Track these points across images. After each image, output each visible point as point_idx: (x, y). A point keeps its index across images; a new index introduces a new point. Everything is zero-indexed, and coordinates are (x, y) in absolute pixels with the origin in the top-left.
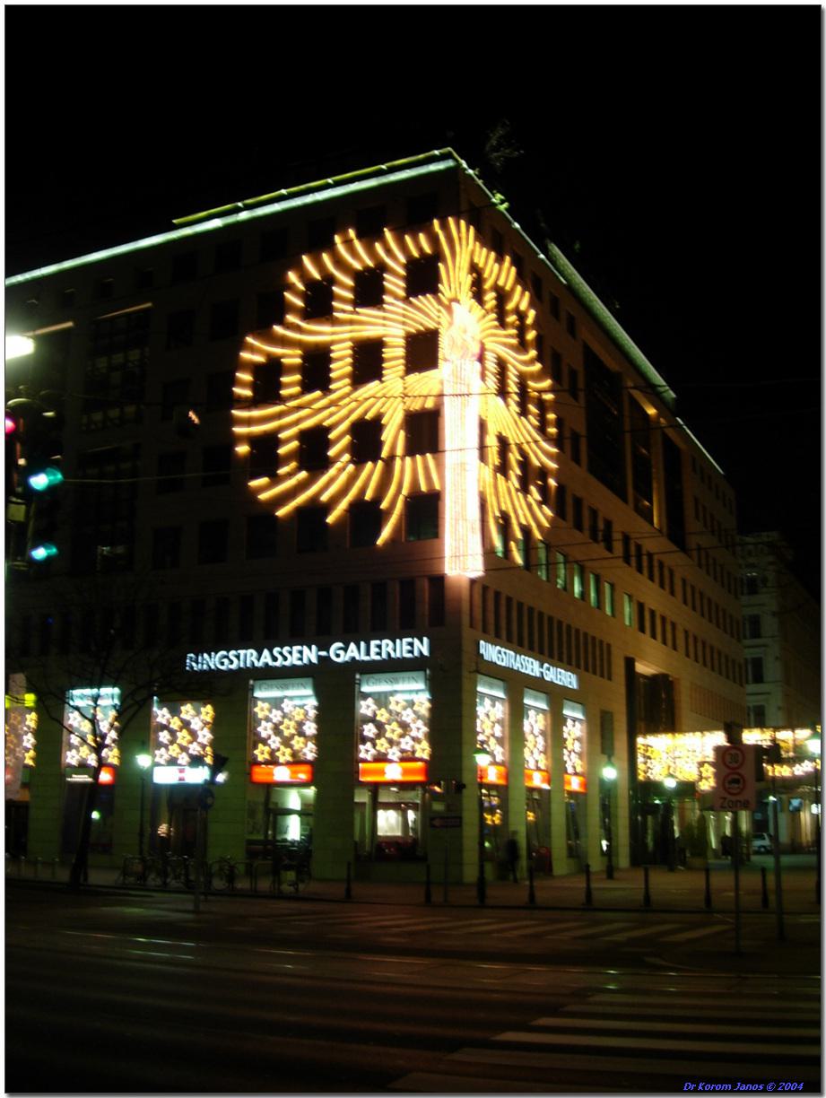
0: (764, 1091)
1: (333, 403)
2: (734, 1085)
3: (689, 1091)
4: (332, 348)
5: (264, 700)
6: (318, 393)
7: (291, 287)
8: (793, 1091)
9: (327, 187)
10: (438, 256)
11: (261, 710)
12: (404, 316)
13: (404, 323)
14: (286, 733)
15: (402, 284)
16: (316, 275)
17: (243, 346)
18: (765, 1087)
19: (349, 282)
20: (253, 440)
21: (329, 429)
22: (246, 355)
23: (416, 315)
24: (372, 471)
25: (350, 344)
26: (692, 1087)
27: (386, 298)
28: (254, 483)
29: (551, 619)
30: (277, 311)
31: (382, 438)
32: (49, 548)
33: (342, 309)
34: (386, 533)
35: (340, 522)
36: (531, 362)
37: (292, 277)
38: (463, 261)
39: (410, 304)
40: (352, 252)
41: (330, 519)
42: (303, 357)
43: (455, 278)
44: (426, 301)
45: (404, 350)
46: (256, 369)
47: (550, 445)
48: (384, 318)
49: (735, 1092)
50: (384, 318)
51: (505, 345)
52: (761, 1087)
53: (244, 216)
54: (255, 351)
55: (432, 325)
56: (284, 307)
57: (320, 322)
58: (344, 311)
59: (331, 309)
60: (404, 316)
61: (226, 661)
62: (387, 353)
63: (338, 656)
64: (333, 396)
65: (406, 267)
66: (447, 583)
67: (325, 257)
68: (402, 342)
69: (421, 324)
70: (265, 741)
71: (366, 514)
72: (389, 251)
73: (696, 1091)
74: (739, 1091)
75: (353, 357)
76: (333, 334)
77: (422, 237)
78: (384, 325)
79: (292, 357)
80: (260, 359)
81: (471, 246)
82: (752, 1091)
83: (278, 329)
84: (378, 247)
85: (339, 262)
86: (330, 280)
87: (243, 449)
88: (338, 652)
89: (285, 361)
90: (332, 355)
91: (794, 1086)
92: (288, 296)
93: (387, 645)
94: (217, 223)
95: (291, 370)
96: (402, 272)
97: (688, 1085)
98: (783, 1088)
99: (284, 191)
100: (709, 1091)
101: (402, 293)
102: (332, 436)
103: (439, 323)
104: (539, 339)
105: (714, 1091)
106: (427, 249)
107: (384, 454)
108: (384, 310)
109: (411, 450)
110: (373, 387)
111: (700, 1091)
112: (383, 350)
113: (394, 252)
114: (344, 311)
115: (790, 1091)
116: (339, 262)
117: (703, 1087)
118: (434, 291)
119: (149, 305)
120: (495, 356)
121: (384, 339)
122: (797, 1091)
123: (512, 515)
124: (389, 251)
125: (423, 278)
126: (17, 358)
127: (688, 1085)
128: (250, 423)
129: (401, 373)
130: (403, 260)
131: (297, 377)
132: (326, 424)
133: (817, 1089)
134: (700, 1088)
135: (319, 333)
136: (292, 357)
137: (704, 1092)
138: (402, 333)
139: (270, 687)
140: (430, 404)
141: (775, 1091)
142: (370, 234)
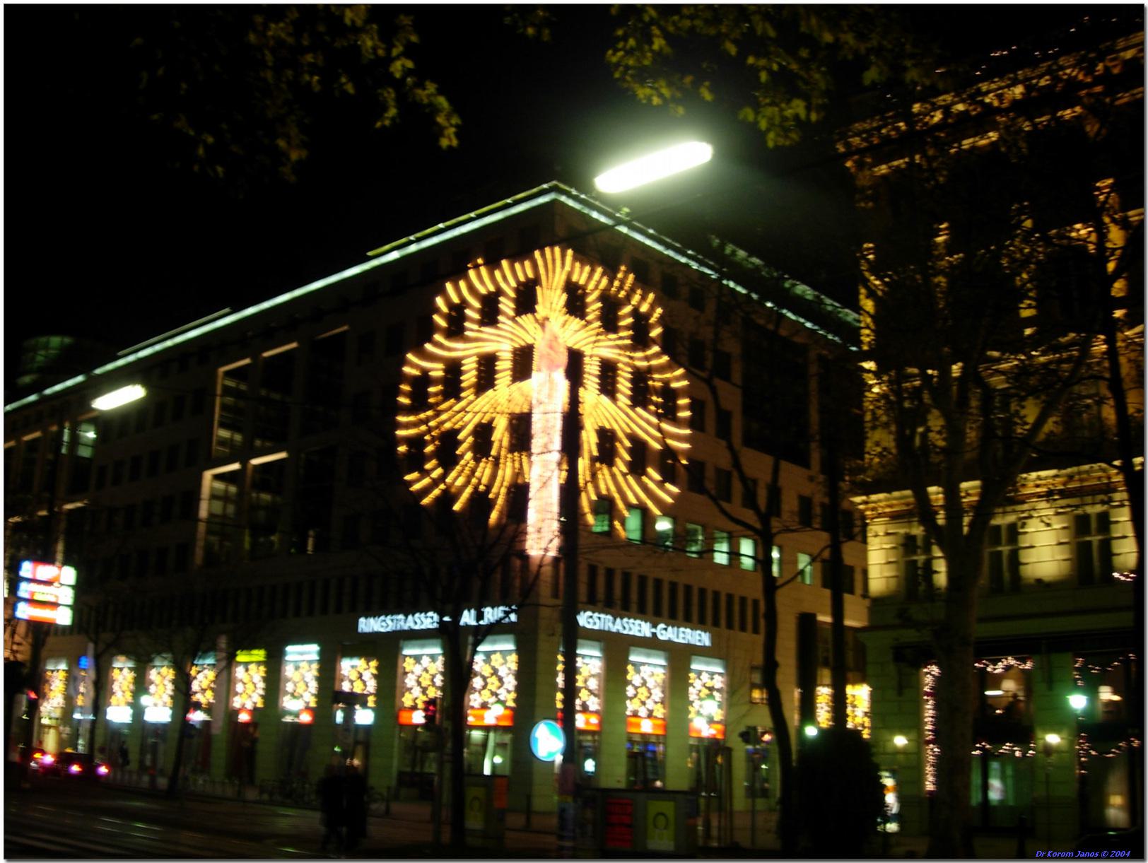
0: (1099, 858)
1: (463, 409)
2: (1076, 853)
3: (1040, 858)
4: (463, 362)
5: (410, 656)
6: (453, 401)
7: (437, 311)
8: (1121, 858)
9: (471, 220)
10: (536, 281)
11: (409, 664)
12: (512, 333)
13: (512, 340)
14: (424, 684)
15: (512, 305)
16: (456, 300)
17: (405, 362)
18: (1100, 855)
19: (477, 304)
20: (408, 441)
21: (459, 431)
22: (407, 369)
23: (518, 331)
24: (485, 470)
25: (475, 359)
26: (1042, 854)
27: (500, 318)
28: (408, 477)
29: (643, 580)
30: (427, 331)
31: (493, 439)
32: (456, 489)
33: (471, 328)
34: (494, 516)
35: (464, 509)
36: (657, 355)
37: (440, 301)
38: (559, 279)
39: (516, 322)
40: (481, 279)
41: (457, 507)
42: (445, 371)
43: (551, 299)
44: (526, 320)
45: (496, 368)
46: (414, 381)
47: (684, 429)
48: (499, 336)
49: (1077, 858)
50: (499, 336)
51: (619, 347)
52: (1097, 855)
53: (413, 248)
54: (413, 365)
55: (530, 341)
56: (433, 328)
57: (457, 341)
58: (472, 330)
59: (463, 329)
60: (512, 333)
61: (384, 624)
62: (500, 365)
64: (463, 403)
65: (517, 290)
66: (531, 560)
67: (462, 284)
68: (509, 356)
69: (523, 340)
70: (410, 690)
71: (481, 501)
72: (504, 278)
73: (1045, 858)
74: (1079, 858)
75: (478, 370)
76: (464, 350)
77: (527, 263)
78: (498, 342)
79: (437, 370)
80: (415, 372)
81: (568, 268)
82: (1090, 858)
83: (428, 346)
84: (497, 274)
85: (472, 289)
86: (464, 304)
87: (402, 449)
89: (431, 374)
90: (463, 368)
91: (1121, 854)
92: (436, 318)
94: (395, 255)
95: (434, 382)
96: (512, 295)
97: (1039, 853)
98: (1114, 855)
99: (441, 226)
100: (1056, 858)
101: (512, 313)
102: (461, 436)
103: (535, 339)
104: (663, 335)
105: (1059, 858)
106: (530, 275)
107: (493, 452)
108: (497, 328)
109: (512, 449)
110: (524, 385)
111: (1049, 858)
112: (496, 363)
113: (509, 276)
114: (472, 330)
115: (1119, 858)
116: (472, 289)
117: (1051, 854)
118: (533, 311)
119: (345, 328)
120: (598, 359)
121: (497, 354)
122: (1125, 858)
123: (617, 496)
124: (504, 278)
125: (526, 300)
126: (138, 400)
127: (1039, 853)
128: (407, 427)
129: (509, 382)
130: (514, 284)
131: (440, 388)
132: (457, 426)
133: (1141, 856)
134: (1049, 855)
135: (458, 349)
136: (437, 370)
137: (1051, 858)
138: (510, 349)
139: (413, 646)
140: (526, 410)
141: (1108, 858)
142: (493, 264)
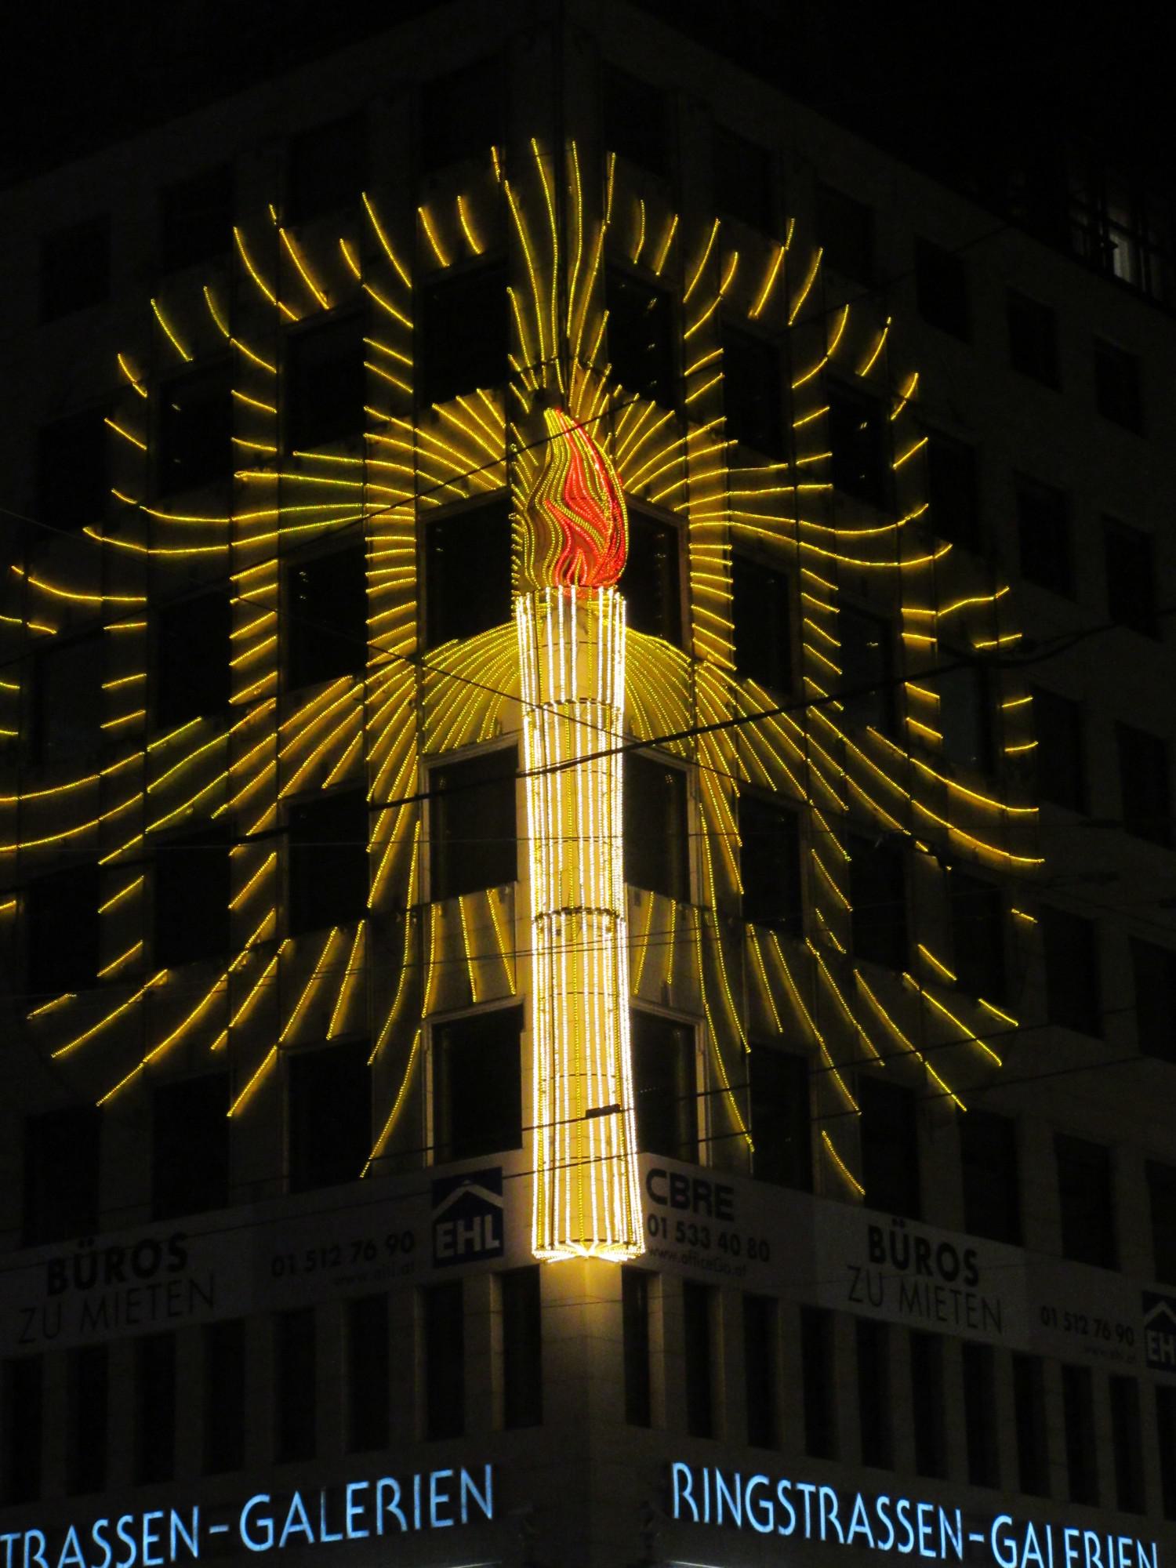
63: (258, 1535)
88: (261, 1523)
93: (388, 1492)
